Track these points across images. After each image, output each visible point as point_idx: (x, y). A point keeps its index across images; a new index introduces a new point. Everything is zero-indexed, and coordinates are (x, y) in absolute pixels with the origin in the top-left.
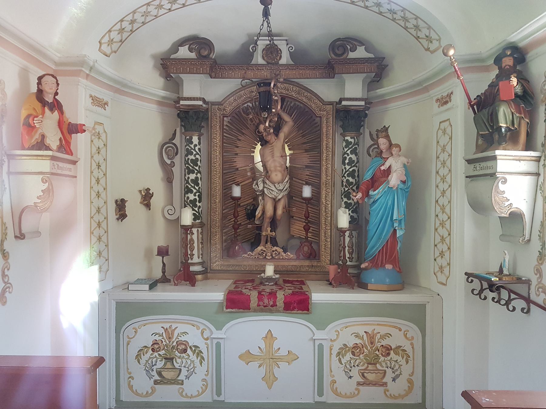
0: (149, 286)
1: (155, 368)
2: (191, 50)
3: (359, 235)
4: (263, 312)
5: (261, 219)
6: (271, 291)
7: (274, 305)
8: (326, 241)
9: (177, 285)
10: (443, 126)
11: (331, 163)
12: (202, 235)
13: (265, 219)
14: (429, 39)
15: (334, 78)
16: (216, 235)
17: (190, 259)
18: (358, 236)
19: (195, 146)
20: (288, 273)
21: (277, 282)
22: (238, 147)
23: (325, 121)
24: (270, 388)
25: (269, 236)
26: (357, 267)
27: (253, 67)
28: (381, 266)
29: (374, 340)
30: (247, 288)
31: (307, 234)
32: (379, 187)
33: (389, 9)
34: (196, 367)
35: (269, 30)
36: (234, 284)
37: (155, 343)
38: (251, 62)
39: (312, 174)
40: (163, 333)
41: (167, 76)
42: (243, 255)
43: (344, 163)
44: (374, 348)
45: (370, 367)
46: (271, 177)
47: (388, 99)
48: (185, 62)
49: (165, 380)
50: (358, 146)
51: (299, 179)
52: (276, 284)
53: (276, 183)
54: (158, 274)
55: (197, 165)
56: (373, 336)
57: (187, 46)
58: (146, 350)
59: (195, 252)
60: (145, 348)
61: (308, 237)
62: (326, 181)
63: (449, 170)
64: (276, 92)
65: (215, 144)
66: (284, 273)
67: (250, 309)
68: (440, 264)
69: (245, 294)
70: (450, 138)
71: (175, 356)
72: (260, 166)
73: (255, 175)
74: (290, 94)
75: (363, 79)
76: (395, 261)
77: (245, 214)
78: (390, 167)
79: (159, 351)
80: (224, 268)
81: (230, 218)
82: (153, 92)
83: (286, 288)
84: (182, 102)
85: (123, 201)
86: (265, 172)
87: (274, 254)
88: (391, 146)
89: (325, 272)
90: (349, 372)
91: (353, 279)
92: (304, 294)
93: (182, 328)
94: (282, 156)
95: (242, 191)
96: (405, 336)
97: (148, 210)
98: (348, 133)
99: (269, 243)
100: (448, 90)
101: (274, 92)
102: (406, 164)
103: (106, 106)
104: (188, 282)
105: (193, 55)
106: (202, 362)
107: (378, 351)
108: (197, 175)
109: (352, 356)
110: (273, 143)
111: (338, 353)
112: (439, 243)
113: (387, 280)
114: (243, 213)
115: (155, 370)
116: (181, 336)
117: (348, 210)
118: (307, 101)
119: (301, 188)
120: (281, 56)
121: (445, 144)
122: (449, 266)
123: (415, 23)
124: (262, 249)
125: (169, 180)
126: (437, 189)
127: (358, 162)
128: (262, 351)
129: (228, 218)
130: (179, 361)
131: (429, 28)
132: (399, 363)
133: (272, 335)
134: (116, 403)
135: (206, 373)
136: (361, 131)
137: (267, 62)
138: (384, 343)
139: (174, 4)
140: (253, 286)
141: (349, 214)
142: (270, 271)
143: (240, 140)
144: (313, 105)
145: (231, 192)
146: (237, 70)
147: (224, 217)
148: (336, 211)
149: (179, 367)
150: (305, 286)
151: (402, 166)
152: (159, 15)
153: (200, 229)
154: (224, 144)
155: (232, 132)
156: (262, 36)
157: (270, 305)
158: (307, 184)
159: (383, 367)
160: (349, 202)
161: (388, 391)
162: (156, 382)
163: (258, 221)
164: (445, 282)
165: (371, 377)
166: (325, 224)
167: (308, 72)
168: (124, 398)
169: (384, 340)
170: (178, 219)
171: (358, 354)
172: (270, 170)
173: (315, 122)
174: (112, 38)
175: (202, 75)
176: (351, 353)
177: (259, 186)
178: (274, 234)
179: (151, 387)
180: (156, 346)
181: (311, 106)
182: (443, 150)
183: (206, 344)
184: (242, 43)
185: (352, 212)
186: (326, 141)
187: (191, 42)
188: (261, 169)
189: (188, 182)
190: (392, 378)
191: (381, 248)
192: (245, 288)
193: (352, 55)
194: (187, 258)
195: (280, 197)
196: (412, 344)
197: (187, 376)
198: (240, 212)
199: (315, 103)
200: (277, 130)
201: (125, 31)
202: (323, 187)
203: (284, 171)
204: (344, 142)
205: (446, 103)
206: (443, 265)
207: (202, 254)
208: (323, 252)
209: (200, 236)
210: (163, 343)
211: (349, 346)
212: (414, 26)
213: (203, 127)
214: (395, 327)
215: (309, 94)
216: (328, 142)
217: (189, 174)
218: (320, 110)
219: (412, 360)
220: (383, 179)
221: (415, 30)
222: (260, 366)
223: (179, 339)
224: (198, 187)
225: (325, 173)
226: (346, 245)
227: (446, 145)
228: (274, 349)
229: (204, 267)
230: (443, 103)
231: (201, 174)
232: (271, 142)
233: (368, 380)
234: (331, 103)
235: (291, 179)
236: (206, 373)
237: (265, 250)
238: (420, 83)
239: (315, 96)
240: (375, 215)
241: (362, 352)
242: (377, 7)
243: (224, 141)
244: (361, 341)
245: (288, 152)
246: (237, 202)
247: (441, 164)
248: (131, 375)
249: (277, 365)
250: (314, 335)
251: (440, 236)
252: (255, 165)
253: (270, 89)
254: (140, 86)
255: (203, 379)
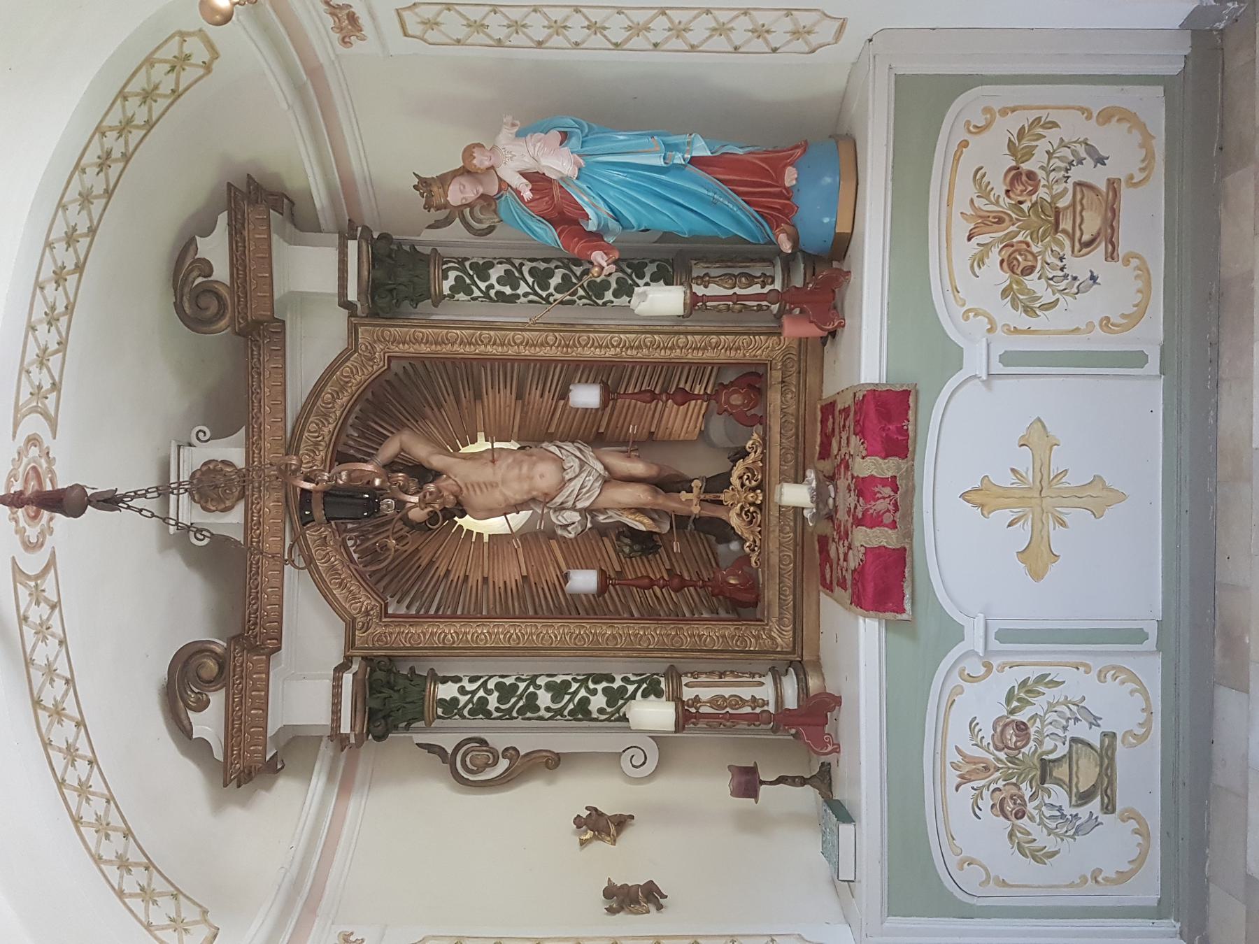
0: (844, 822)
1: (1068, 811)
2: (202, 705)
3: (704, 258)
4: (912, 513)
5: (656, 517)
6: (852, 493)
7: (893, 483)
8: (717, 346)
9: (839, 745)
10: (414, 28)
11: (513, 333)
12: (700, 673)
13: (656, 508)
14: (180, 63)
15: (284, 322)
16: (700, 636)
17: (766, 708)
18: (706, 262)
19: (462, 691)
20: (801, 446)
21: (827, 475)
22: (466, 577)
23: (401, 345)
24: (1122, 497)
25: (702, 497)
26: (788, 263)
27: (252, 537)
28: (789, 199)
29: (994, 214)
30: (846, 555)
31: (697, 397)
32: (576, 203)
33: (97, 170)
34: (1066, 698)
35: (155, 494)
36: (832, 591)
37: (999, 807)
38: (239, 542)
39: (537, 384)
40: (973, 788)
41: (272, 769)
42: (753, 564)
43: (512, 299)
44: (1014, 216)
45: (1066, 224)
46: (546, 491)
47: (340, 177)
48: (233, 721)
49: (1102, 785)
50: (468, 259)
51: (553, 415)
52: (832, 479)
53: (563, 478)
54: (808, 796)
55: (514, 687)
56: (981, 217)
57: (191, 714)
58: (1020, 832)
59: (746, 693)
60: (1013, 838)
61: (705, 393)
62: (559, 345)
63: (535, 11)
64: (326, 476)
65: (458, 638)
66: (801, 459)
67: (905, 549)
68: (788, 37)
69: (861, 560)
70: (449, 10)
71: (1036, 755)
72: (518, 520)
73: (543, 532)
74: (327, 439)
75: (286, 244)
76: (775, 163)
77: (644, 557)
78: (524, 175)
79: (1022, 798)
80: (790, 617)
81: (652, 600)
82: (313, 810)
83: (843, 450)
84: (345, 728)
85: (610, 892)
86: (532, 506)
87: (750, 482)
88: (469, 172)
89: (800, 350)
90: (1077, 283)
91: (823, 273)
92: (860, 404)
93: (958, 736)
94: (493, 461)
95: (583, 566)
96: (980, 130)
97: (633, 821)
98: (433, 285)
99: (722, 497)
100: (317, 11)
101: (327, 482)
102: (516, 129)
103: (352, 938)
104: (829, 714)
105: (217, 699)
106: (1052, 681)
107: (1021, 202)
108: (539, 687)
109: (1035, 275)
110: (458, 485)
111: (1026, 312)
112: (729, 39)
113: (828, 180)
114: (641, 565)
115: (1074, 811)
116: (979, 737)
117: (636, 289)
118: (346, 394)
119: (577, 412)
120: (222, 461)
121: (465, 23)
122: (793, 12)
123: (137, 100)
124: (737, 514)
125: (551, 762)
126: (584, 46)
127: (509, 261)
128: (1022, 516)
129: (654, 603)
130: (1048, 744)
131: (150, 62)
132: (1055, 148)
133: (976, 490)
134: (1166, 918)
135: (1082, 669)
136: (427, 250)
137: (239, 499)
138: (1000, 188)
139: (77, 750)
140: (840, 539)
141: (647, 284)
142: (796, 495)
143: (448, 572)
144: (358, 378)
145: (586, 595)
146: (259, 580)
147: (650, 615)
148: (639, 319)
149: (1067, 743)
150: (838, 401)
151: (521, 142)
152: (106, 792)
153: (685, 680)
154: (459, 612)
155: (426, 595)
156: (168, 512)
157: (892, 494)
158: (564, 395)
159: (1066, 190)
160: (614, 285)
161: (1131, 177)
162: (1107, 808)
163: (663, 525)
164: (837, 24)
165: (1092, 224)
166: (671, 349)
167: (267, 390)
168: (1151, 897)
169: (992, 189)
170: (658, 738)
171: (1030, 257)
172: (529, 492)
173: (401, 372)
174: (168, 922)
175: (271, 673)
176: (1026, 278)
177: (569, 521)
178: (696, 484)
179: (1123, 821)
180: (1010, 806)
181: (360, 384)
182: (480, 27)
183: (1002, 670)
184: (187, 569)
185: (641, 277)
186: (453, 344)
187: (181, 704)
188: (524, 515)
189: (560, 712)
190: (1095, 166)
191: (739, 199)
192: (845, 560)
193: (221, 272)
194: (764, 715)
195: (600, 467)
196: (1004, 112)
197: (1091, 724)
198: (638, 570)
199: (352, 372)
200: (422, 474)
201: (149, 885)
202: (574, 354)
203: (531, 455)
204: (457, 296)
205: (352, 18)
206: (789, 29)
207: (751, 673)
208: (745, 355)
209: (703, 679)
210: (1001, 787)
211: (1008, 282)
212: (145, 102)
213: (412, 670)
214: (957, 158)
215: (328, 389)
216: (457, 340)
217: (537, 709)
218: (371, 359)
219: (1046, 111)
220: (557, 193)
221: (156, 101)
222: (1063, 524)
223: (989, 744)
224: (573, 684)
225: (538, 349)
226: (730, 292)
227: (468, 19)
228: (1014, 486)
229: (787, 670)
230: (353, 26)
231: (536, 677)
232: (456, 488)
233: (1100, 229)
234: (353, 331)
235: (551, 438)
236: (1082, 669)
237: (739, 505)
238: (299, 89)
239: (333, 374)
240: (650, 216)
241: (1024, 246)
242: (92, 203)
243: (449, 613)
244: (995, 250)
245: (481, 445)
246: (612, 579)
247: (517, 33)
248: (1089, 877)
249: (1061, 476)
250: (975, 377)
251: (711, 36)
252: (514, 531)
253: (317, 492)
254: (298, 845)
255: (1099, 676)
